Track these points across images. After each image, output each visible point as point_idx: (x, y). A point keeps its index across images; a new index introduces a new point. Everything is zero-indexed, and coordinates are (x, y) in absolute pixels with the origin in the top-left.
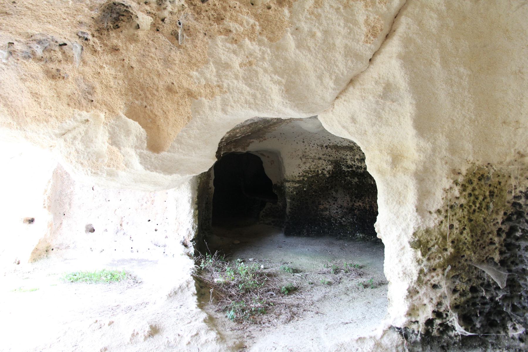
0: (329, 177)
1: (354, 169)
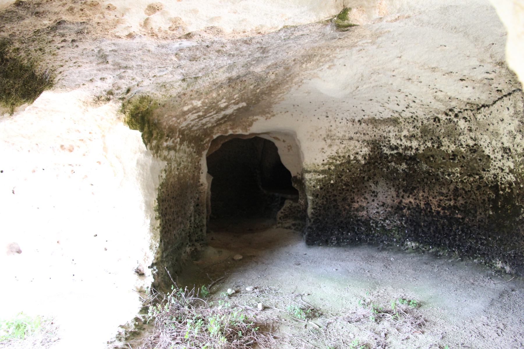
0: (365, 164)
1: (401, 151)
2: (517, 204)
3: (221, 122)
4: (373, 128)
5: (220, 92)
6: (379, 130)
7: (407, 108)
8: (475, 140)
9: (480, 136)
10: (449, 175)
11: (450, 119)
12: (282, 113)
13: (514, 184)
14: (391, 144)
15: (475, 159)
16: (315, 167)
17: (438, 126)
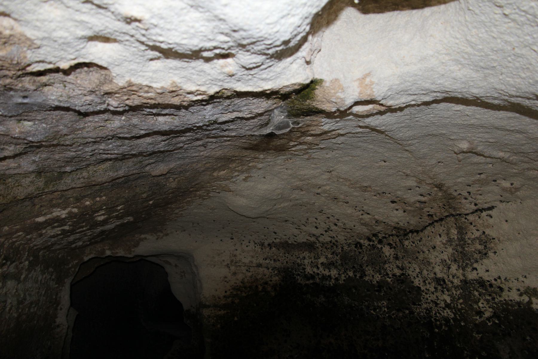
1: (318, 280)
2: (459, 345)
4: (285, 253)
6: (292, 256)
7: (326, 231)
10: (375, 310)
11: (373, 245)
13: (452, 321)
14: (307, 273)
17: (360, 253)
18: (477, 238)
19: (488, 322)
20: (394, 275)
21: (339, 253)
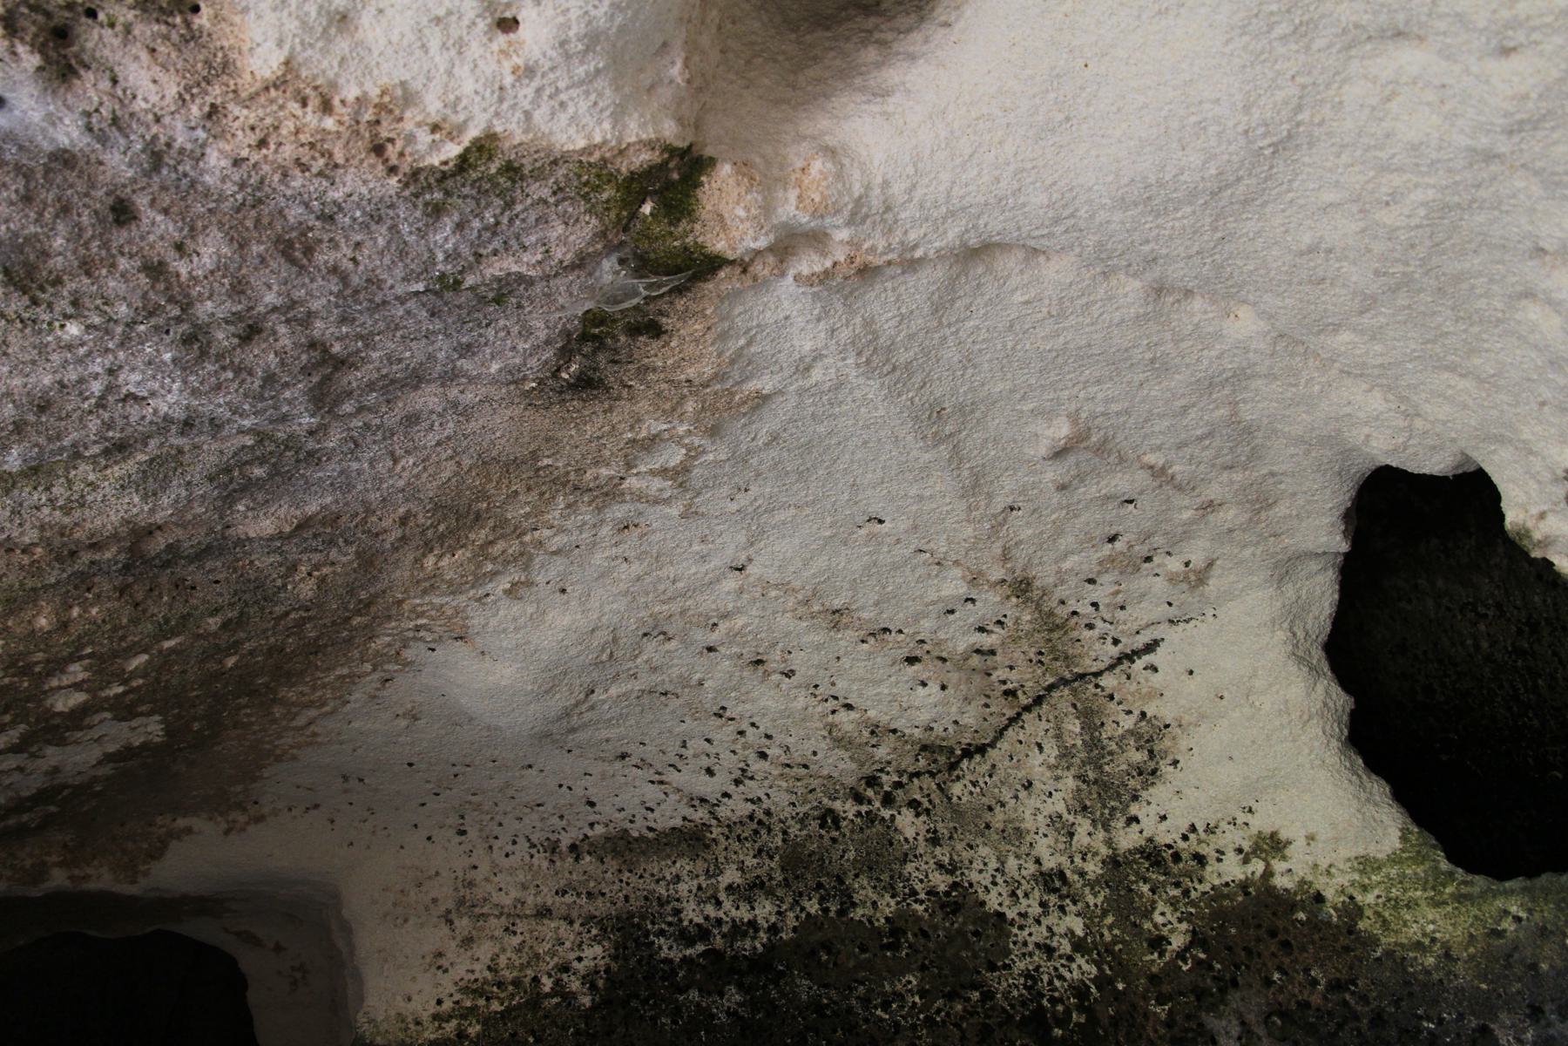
0: (595, 1007)
1: (719, 942)
3: (25, 818)
4: (620, 871)
5: (75, 612)
6: (641, 877)
7: (737, 782)
8: (951, 872)
9: (966, 855)
10: (886, 1006)
12: (294, 812)
13: (1093, 990)
14: (686, 923)
15: (961, 932)
16: (406, 1029)
17: (834, 840)
18: (1128, 731)
19: (1180, 963)
20: (931, 892)
21: (777, 848)
